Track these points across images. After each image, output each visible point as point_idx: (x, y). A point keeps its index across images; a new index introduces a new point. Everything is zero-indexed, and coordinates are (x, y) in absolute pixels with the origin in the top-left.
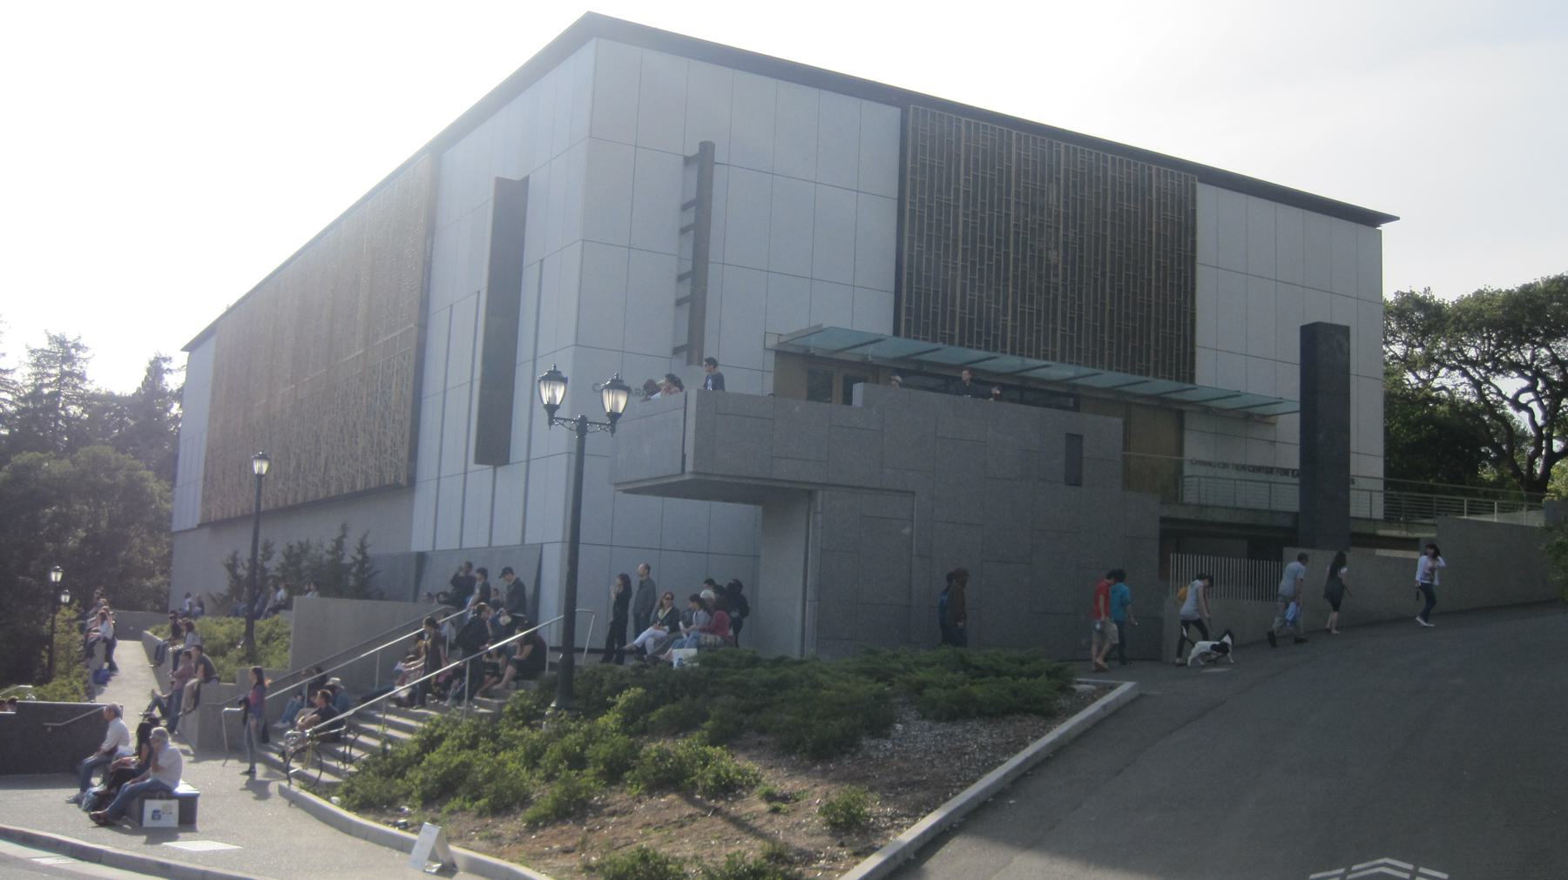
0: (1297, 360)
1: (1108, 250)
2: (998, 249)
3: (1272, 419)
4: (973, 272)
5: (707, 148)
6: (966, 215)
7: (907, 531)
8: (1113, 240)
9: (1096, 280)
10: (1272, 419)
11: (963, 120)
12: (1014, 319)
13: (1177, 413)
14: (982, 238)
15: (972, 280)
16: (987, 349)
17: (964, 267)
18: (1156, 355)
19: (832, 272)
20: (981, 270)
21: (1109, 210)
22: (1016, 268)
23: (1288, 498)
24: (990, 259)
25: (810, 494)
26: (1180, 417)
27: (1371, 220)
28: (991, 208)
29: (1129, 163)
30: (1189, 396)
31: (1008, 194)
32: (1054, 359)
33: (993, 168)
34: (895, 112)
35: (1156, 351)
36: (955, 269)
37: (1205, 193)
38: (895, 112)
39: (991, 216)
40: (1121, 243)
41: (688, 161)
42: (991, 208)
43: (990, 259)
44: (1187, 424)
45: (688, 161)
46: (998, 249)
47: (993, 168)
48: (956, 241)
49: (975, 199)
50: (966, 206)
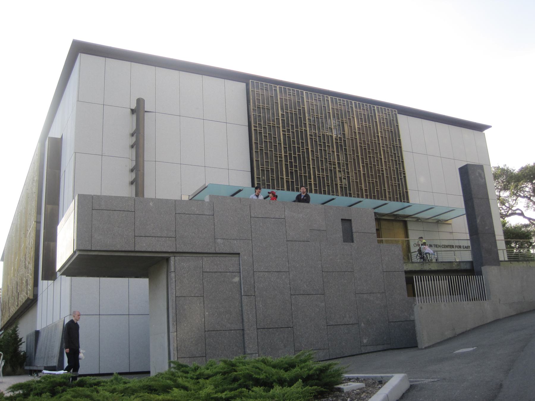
0: (461, 194)
1: (359, 145)
2: (303, 147)
3: (449, 222)
4: (291, 159)
5: (140, 102)
6: (283, 131)
7: (237, 279)
8: (360, 140)
9: (354, 159)
10: (449, 222)
11: (278, 86)
12: (315, 180)
13: (402, 221)
14: (294, 142)
15: (291, 162)
16: (358, 197)
17: (286, 156)
18: (389, 194)
19: (206, 159)
20: (295, 157)
21: (356, 127)
22: (313, 154)
23: (467, 256)
24: (299, 151)
25: (167, 259)
26: (405, 223)
27: (480, 128)
28: (297, 127)
29: (363, 105)
30: (408, 212)
31: (305, 120)
32: (363, 197)
33: (295, 109)
34: (243, 85)
35: (389, 192)
36: (281, 157)
37: (402, 120)
38: (243, 85)
39: (297, 131)
40: (364, 141)
41: (133, 111)
42: (297, 127)
43: (299, 151)
44: (409, 227)
45: (133, 111)
46: (303, 147)
47: (295, 109)
48: (280, 144)
49: (288, 124)
50: (284, 127)
